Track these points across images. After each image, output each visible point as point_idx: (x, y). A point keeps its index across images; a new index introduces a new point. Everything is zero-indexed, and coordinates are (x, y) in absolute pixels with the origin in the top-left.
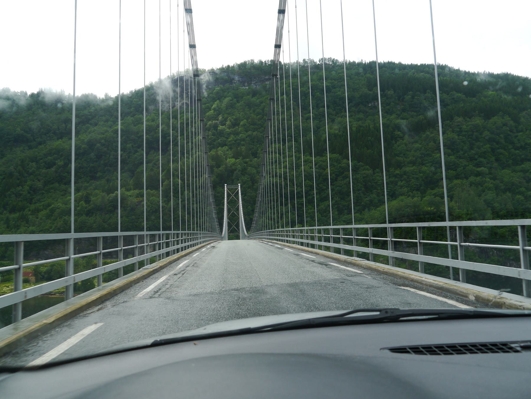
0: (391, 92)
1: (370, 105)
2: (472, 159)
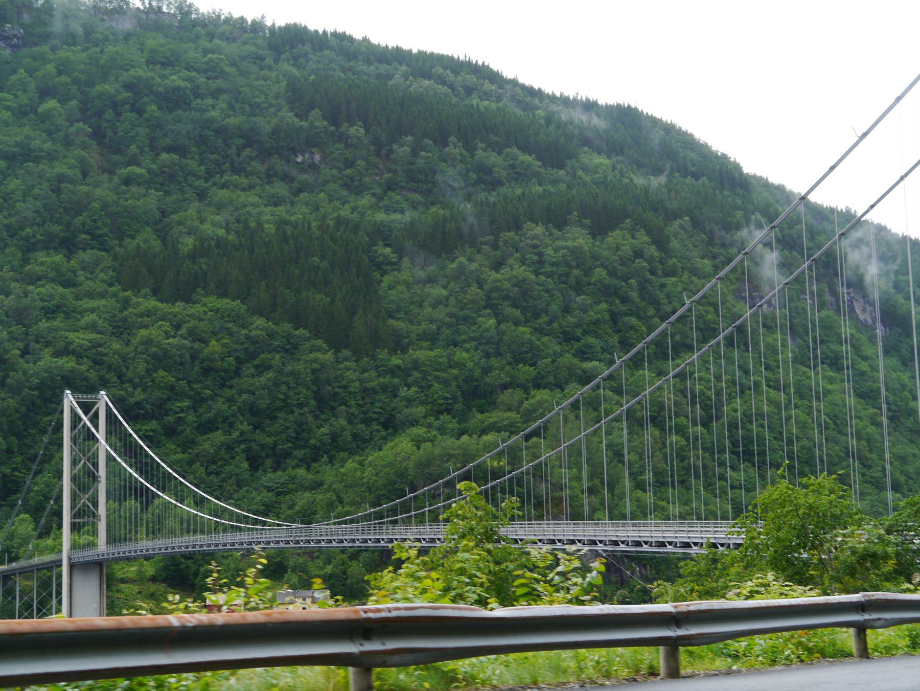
0: (357, 130)
1: (299, 159)
2: (568, 337)
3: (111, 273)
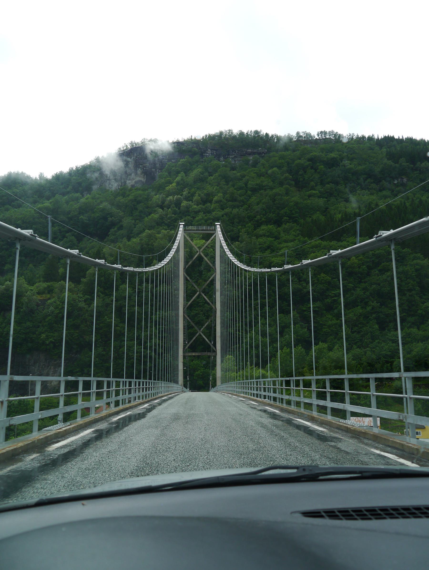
1: (396, 182)
3: (298, 232)
